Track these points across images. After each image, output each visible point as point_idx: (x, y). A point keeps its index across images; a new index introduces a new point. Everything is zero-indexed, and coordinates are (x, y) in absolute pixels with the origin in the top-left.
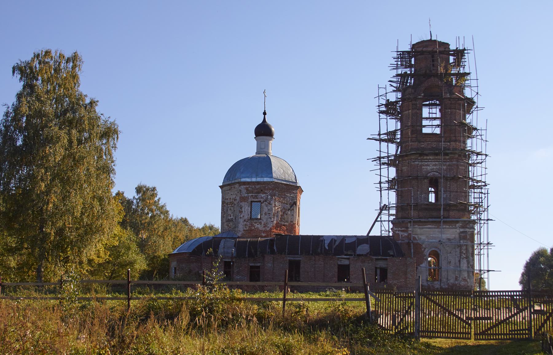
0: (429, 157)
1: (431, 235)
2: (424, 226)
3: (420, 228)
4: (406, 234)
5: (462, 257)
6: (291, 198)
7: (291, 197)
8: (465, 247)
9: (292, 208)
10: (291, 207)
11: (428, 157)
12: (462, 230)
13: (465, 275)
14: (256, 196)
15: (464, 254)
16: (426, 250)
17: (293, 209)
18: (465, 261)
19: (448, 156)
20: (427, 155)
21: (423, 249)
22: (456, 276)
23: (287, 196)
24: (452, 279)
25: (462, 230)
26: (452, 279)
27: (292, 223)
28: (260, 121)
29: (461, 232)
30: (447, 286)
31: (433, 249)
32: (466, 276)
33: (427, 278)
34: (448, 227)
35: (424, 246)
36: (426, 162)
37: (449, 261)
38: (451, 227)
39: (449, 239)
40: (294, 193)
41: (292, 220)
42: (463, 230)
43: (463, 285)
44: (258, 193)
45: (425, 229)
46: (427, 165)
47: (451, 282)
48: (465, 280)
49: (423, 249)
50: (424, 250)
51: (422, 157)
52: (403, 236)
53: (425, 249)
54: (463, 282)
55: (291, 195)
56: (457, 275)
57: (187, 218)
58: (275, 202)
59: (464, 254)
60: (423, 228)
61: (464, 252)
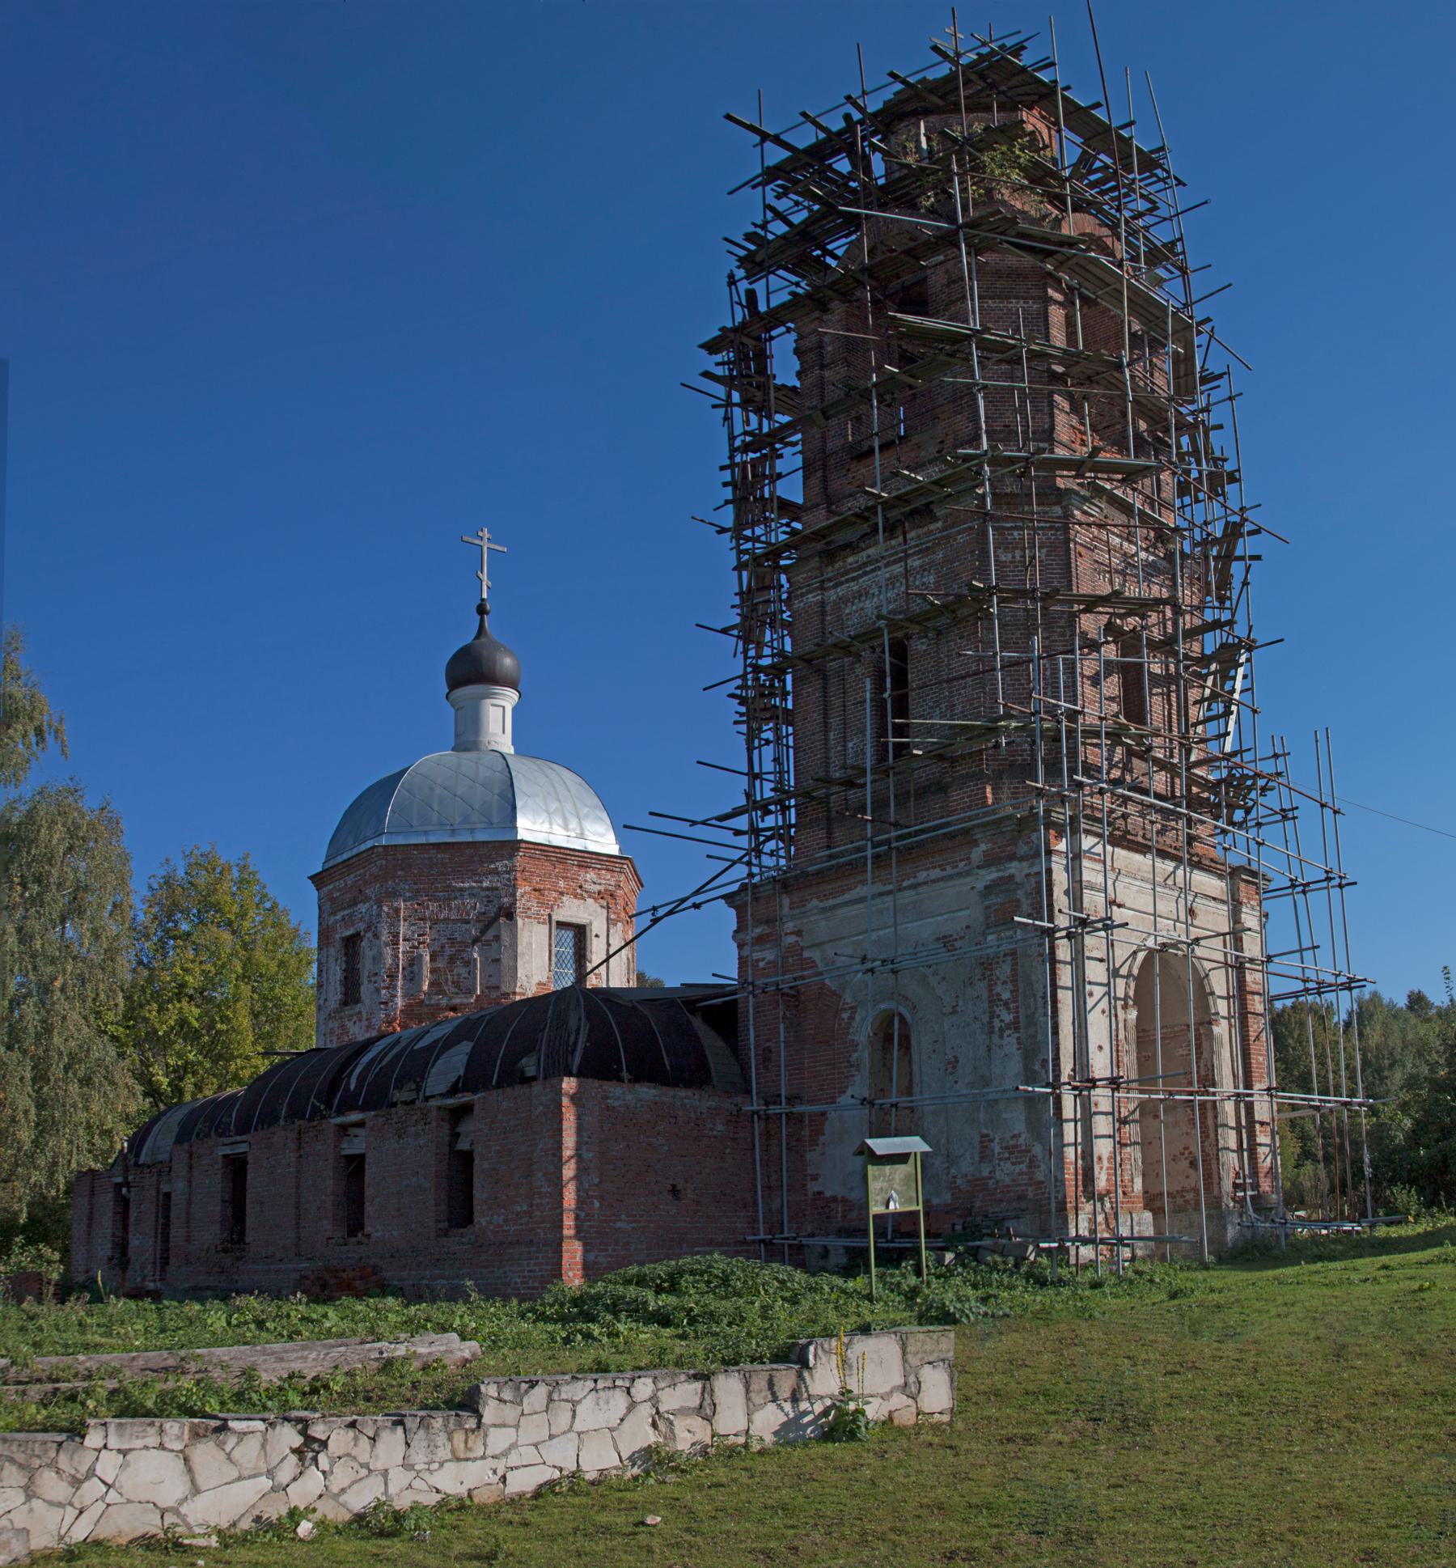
0: (864, 554)
1: (874, 936)
2: (843, 892)
3: (824, 910)
4: (769, 955)
5: (997, 1023)
6: (483, 894)
7: (487, 889)
8: (1007, 969)
9: (490, 934)
10: (483, 931)
11: (863, 556)
12: (990, 875)
13: (1016, 1120)
14: (351, 916)
15: (1006, 1004)
16: (858, 1018)
17: (497, 938)
18: (1010, 1042)
19: (935, 519)
20: (852, 547)
21: (845, 1016)
22: (982, 1136)
23: (461, 890)
24: (968, 1155)
25: (990, 875)
26: (968, 1155)
27: (494, 995)
28: (468, 639)
29: (989, 889)
30: (948, 1197)
31: (883, 1006)
32: (1020, 1127)
33: (129, 1191)
34: (936, 873)
35: (848, 998)
36: (853, 579)
37: (950, 1057)
38: (949, 871)
39: (946, 942)
40: (496, 872)
41: (494, 981)
42: (994, 876)
43: (1007, 1179)
44: (354, 903)
45: (841, 912)
46: (861, 594)
47: (964, 1170)
48: (1013, 1151)
49: (845, 1016)
50: (852, 1018)
51: (840, 563)
52: (761, 964)
53: (854, 1009)
54: (1007, 1166)
55: (481, 882)
56: (985, 1131)
57: (1422, 990)
58: (391, 925)
59: (1006, 1004)
60: (834, 907)
61: (1006, 996)
